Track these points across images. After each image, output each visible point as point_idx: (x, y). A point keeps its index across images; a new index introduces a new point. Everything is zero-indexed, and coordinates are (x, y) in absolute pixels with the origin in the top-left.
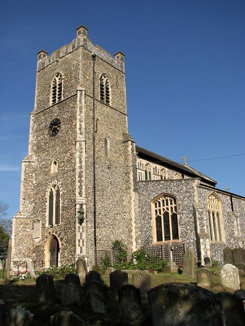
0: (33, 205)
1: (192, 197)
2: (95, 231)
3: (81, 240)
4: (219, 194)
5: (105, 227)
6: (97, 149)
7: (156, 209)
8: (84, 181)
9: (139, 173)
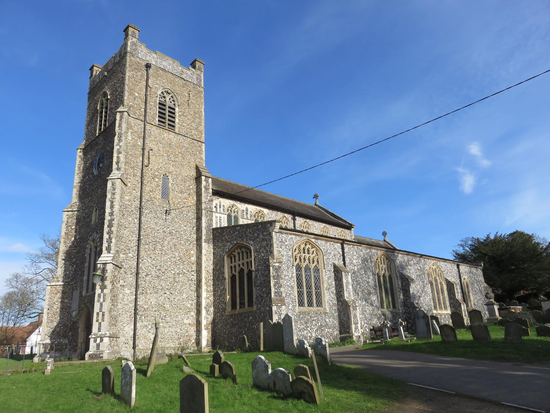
0: (75, 266)
1: (269, 246)
2: (136, 299)
3: (101, 314)
4: (319, 241)
5: (157, 293)
6: (147, 189)
7: (231, 265)
8: (114, 232)
9: (216, 217)
